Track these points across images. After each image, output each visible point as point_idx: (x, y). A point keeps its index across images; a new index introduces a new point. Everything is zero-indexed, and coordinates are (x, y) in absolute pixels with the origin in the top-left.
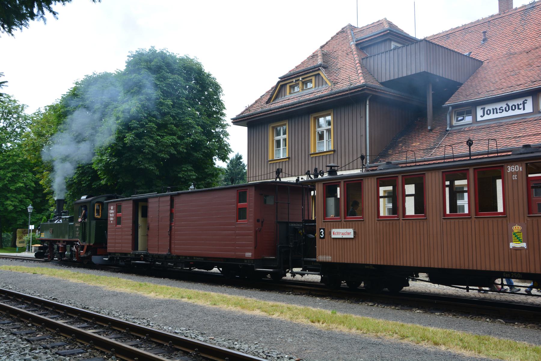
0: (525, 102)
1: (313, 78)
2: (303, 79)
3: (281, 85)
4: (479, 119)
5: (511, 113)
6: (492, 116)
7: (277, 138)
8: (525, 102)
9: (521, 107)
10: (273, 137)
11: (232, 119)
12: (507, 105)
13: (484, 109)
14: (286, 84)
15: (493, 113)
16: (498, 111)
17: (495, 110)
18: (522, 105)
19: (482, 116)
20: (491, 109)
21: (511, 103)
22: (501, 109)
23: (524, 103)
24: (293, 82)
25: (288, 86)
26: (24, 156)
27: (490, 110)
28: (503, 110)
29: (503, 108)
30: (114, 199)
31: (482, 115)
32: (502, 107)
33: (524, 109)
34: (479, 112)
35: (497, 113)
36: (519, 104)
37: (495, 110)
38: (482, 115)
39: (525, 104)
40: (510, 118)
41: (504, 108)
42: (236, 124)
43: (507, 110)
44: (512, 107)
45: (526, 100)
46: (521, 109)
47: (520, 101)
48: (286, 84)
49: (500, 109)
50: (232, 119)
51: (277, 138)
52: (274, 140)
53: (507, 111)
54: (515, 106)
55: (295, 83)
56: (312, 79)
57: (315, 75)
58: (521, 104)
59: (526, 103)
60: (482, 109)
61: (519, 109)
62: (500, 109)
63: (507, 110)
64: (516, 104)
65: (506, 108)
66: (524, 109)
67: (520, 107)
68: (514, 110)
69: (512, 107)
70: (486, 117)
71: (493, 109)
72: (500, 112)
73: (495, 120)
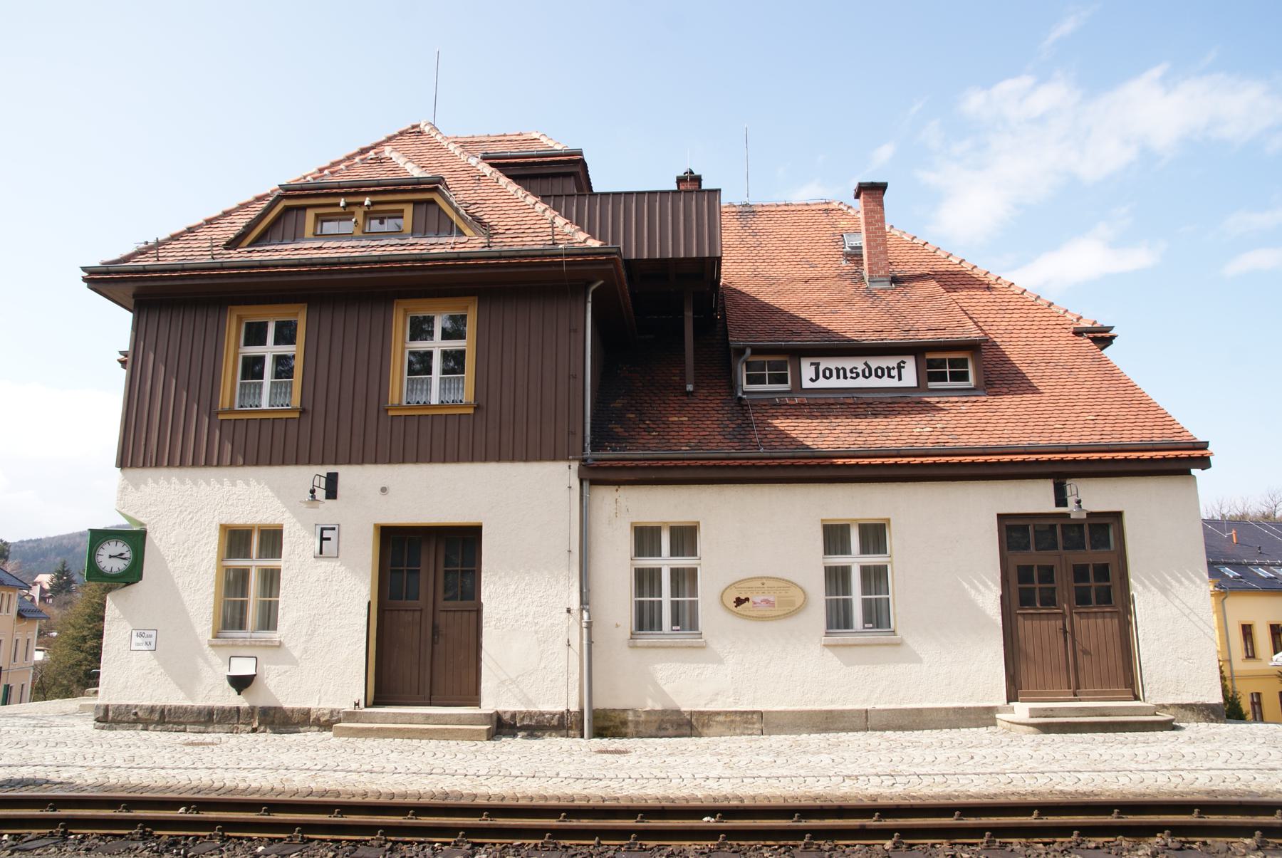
0: (902, 365)
1: (408, 210)
2: (373, 203)
3: (285, 206)
4: (807, 384)
5: (873, 382)
6: (834, 383)
7: (420, 346)
8: (902, 365)
9: (894, 373)
10: (237, 346)
11: (84, 269)
12: (866, 364)
13: (817, 365)
14: (304, 208)
15: (838, 377)
16: (849, 375)
17: (841, 372)
18: (896, 370)
19: (812, 380)
20: (833, 368)
21: (875, 363)
22: (854, 371)
23: (900, 368)
24: (338, 205)
25: (310, 215)
26: (486, 851)
27: (831, 371)
28: (858, 375)
29: (858, 370)
30: (357, 728)
31: (814, 378)
32: (856, 368)
33: (900, 379)
34: (807, 370)
35: (845, 377)
36: (891, 367)
37: (841, 372)
38: (814, 378)
39: (902, 370)
40: (873, 392)
41: (860, 371)
42: (93, 286)
43: (867, 374)
44: (876, 370)
45: (904, 362)
46: (893, 377)
47: (892, 362)
48: (304, 208)
49: (851, 371)
50: (84, 269)
51: (420, 346)
52: (238, 353)
53: (867, 378)
54: (883, 370)
55: (342, 210)
56: (402, 211)
57: (416, 203)
58: (894, 368)
59: (904, 367)
60: (812, 364)
61: (890, 376)
62: (851, 371)
63: (867, 374)
64: (884, 366)
65: (863, 371)
66: (900, 379)
67: (892, 374)
68: (880, 377)
69: (876, 370)
70: (822, 383)
71: (838, 370)
72: (852, 378)
73: (844, 391)
